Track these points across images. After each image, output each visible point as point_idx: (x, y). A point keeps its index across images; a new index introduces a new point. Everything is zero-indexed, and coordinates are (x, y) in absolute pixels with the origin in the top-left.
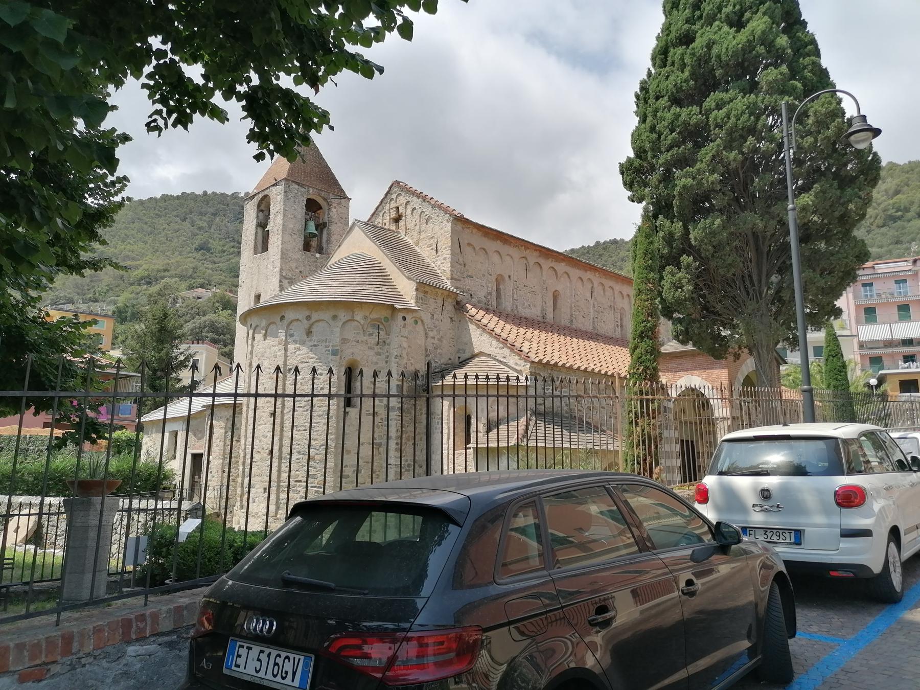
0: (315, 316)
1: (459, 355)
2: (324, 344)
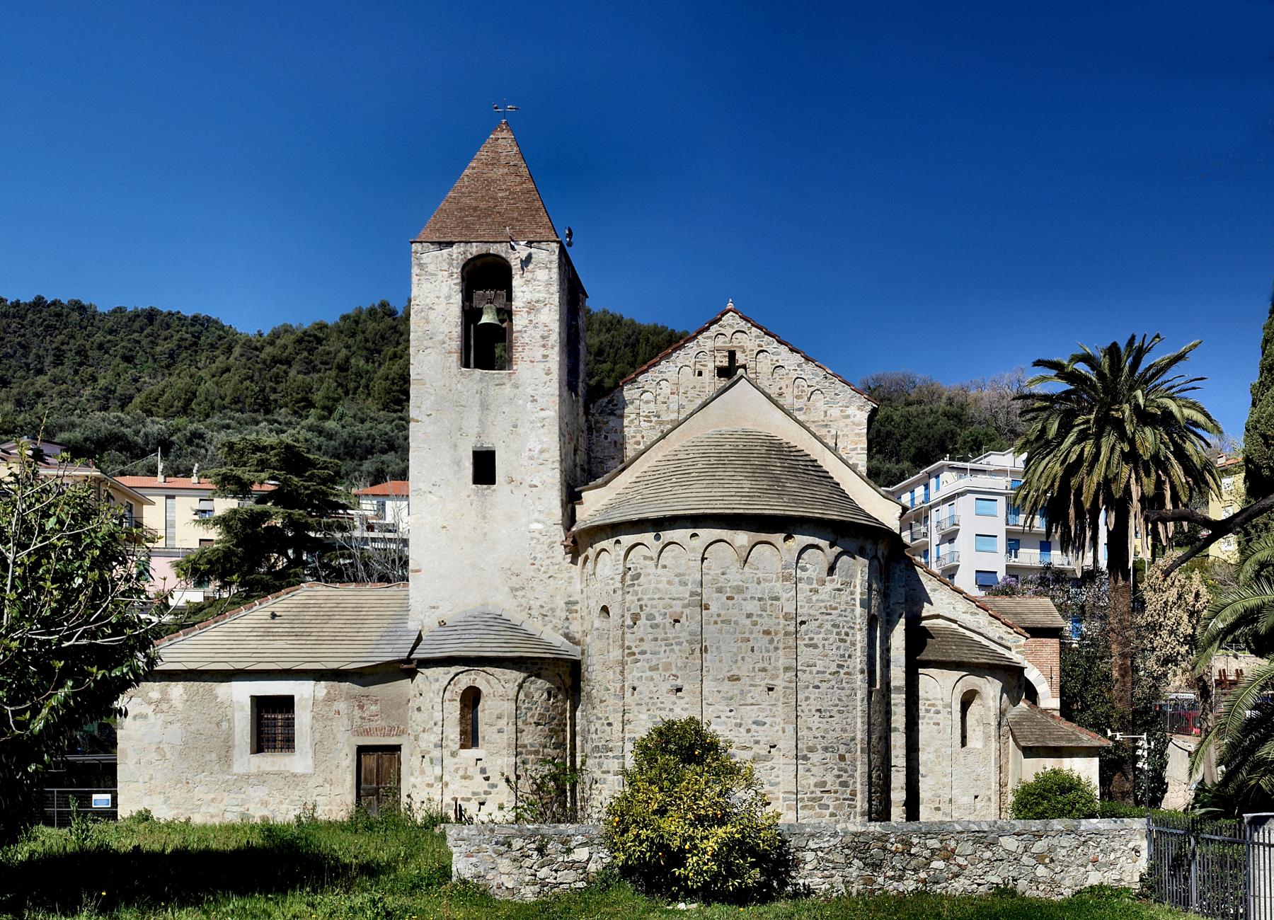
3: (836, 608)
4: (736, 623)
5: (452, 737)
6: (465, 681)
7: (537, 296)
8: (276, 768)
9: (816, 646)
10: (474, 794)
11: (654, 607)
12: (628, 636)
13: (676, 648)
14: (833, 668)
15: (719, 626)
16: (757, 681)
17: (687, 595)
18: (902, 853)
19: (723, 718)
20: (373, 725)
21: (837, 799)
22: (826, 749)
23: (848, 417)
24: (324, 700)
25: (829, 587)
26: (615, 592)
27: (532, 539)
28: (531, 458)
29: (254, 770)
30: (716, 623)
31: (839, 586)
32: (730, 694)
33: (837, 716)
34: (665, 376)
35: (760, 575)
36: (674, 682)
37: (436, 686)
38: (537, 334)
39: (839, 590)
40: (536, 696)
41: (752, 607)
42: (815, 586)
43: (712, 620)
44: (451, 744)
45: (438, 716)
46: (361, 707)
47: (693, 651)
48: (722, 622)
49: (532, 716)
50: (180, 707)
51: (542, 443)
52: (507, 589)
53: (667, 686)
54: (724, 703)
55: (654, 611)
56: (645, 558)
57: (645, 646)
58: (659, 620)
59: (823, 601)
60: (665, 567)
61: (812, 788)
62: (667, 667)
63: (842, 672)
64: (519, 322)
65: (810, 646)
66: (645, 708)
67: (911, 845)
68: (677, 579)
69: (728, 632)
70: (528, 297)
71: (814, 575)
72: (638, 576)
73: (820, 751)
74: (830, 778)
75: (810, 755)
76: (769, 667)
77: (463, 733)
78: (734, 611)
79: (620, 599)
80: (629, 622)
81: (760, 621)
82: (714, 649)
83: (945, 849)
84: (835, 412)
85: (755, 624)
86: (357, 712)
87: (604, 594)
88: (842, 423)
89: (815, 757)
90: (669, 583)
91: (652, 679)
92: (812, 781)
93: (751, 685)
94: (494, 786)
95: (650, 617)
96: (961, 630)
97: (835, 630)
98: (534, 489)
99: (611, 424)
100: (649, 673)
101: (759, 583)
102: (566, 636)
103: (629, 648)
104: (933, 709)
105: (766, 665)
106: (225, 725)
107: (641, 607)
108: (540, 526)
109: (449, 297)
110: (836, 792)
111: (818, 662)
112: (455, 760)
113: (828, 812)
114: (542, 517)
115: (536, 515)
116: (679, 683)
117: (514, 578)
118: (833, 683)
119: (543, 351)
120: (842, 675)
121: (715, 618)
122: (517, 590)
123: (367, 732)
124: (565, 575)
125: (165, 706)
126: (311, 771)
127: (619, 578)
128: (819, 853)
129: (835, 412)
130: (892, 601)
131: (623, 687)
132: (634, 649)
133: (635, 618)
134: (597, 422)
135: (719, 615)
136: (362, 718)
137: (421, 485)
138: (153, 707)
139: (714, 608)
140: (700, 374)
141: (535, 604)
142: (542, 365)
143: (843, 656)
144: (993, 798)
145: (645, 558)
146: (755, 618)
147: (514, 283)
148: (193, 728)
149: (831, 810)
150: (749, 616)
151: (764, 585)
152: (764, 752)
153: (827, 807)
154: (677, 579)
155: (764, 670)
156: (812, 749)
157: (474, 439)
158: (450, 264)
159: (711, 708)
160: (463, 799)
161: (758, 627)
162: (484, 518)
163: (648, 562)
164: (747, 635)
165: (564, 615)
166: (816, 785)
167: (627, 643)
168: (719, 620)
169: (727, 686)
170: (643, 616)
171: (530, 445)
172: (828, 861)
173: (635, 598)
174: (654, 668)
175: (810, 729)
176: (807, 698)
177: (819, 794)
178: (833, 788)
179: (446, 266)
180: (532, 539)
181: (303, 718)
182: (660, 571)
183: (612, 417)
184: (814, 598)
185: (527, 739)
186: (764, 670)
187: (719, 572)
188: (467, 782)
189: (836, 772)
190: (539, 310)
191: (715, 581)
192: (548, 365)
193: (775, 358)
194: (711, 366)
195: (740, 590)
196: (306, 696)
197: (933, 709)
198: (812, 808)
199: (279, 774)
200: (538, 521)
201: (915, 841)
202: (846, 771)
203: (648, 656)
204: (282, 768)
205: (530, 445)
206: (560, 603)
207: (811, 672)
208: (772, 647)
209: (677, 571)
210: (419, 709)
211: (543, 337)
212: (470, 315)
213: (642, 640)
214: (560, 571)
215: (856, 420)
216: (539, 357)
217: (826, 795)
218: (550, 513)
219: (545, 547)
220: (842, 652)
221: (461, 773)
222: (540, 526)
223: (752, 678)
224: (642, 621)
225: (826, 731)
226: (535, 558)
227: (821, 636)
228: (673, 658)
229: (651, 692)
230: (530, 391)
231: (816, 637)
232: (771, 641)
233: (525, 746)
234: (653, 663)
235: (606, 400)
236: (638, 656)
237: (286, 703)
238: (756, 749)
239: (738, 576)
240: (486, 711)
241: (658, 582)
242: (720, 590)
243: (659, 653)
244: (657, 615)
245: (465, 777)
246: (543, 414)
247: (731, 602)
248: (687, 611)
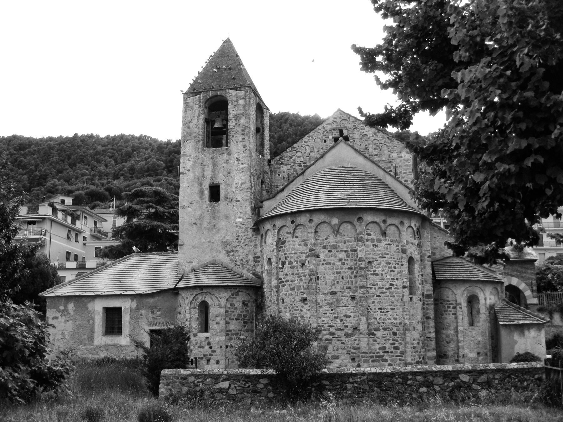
0: (389, 221)
2: (395, 244)
3: (387, 254)
4: (334, 264)
5: (194, 326)
6: (200, 298)
7: (239, 112)
8: (113, 343)
9: (377, 275)
10: (205, 355)
11: (292, 257)
12: (280, 273)
13: (303, 278)
14: (388, 286)
15: (325, 266)
16: (346, 294)
17: (308, 251)
18: (402, 384)
19: (328, 314)
20: (158, 321)
21: (393, 356)
22: (384, 329)
23: (401, 157)
24: (135, 309)
25: (383, 243)
26: (273, 251)
27: (237, 226)
28: (237, 187)
29: (103, 344)
30: (323, 264)
31: (389, 243)
32: (331, 301)
33: (391, 311)
34: (307, 144)
35: (346, 239)
36: (302, 296)
37: (187, 301)
38: (239, 129)
39: (389, 244)
40: (237, 305)
41: (342, 255)
42: (375, 243)
43: (321, 263)
44: (193, 330)
45: (188, 316)
46: (153, 312)
47: (311, 279)
48: (327, 264)
49: (234, 316)
50: (72, 313)
51: (242, 180)
52: (225, 252)
53: (298, 298)
54: (328, 306)
55: (292, 260)
56: (288, 233)
57: (288, 278)
58: (294, 264)
59: (380, 251)
60: (297, 237)
61: (378, 350)
62: (299, 288)
63: (393, 287)
64: (231, 124)
65: (374, 274)
66: (288, 310)
67: (408, 379)
68: (303, 243)
69: (330, 269)
70: (235, 113)
71: (375, 237)
72: (284, 242)
73: (382, 330)
74: (388, 345)
75: (375, 333)
76: (352, 287)
77: (200, 324)
78: (332, 258)
79: (276, 254)
80: (280, 266)
81: (346, 262)
82: (322, 278)
83: (427, 381)
84: (394, 155)
85: (343, 264)
86: (150, 315)
87: (269, 252)
88: (398, 160)
89: (379, 334)
90: (299, 245)
91: (292, 295)
92: (377, 346)
93: (342, 296)
94: (215, 351)
95: (290, 263)
97: (388, 266)
98: (238, 202)
99: (282, 169)
100: (290, 292)
101: (345, 243)
102: (253, 274)
103: (280, 279)
104: (452, 306)
105: (350, 285)
106: (91, 322)
107: (286, 258)
108: (241, 220)
109: (199, 116)
110: (392, 352)
111: (379, 283)
112: (196, 338)
113: (387, 364)
114: (242, 216)
115: (239, 215)
116: (305, 296)
117: (228, 246)
118: (388, 294)
119: (242, 137)
120: (393, 289)
121: (322, 262)
122: (230, 252)
123: (155, 325)
124: (253, 244)
125: (66, 313)
126: (129, 344)
127: (275, 244)
128: (355, 385)
129: (394, 155)
130: (424, 249)
131: (278, 300)
132: (283, 280)
133: (283, 263)
134: (275, 168)
135: (324, 260)
136: (153, 318)
137: (184, 204)
138: (61, 313)
139: (322, 257)
140: (325, 141)
141: (239, 259)
142: (242, 143)
143: (393, 279)
144: (488, 354)
145: (288, 233)
146: (343, 261)
147: (229, 107)
148: (77, 323)
149: (389, 362)
150: (340, 260)
151: (347, 244)
152: (350, 332)
153: (386, 361)
154: (303, 243)
155: (349, 288)
156: (377, 330)
157: (209, 180)
158: (200, 102)
159: (321, 309)
160: (199, 358)
161: (345, 266)
162: (214, 218)
163: (288, 235)
164: (339, 270)
165: (252, 263)
166: (380, 349)
167: (280, 277)
168: (324, 263)
169: (329, 297)
170: (287, 262)
171: (236, 180)
172: (360, 389)
173: (283, 253)
174: (293, 289)
175: (376, 319)
176: (373, 302)
177: (382, 354)
178: (389, 350)
179: (197, 103)
180: (237, 226)
181: (126, 318)
182: (295, 239)
183: (282, 165)
184: (375, 249)
185: (232, 327)
186: (349, 288)
187: (324, 238)
188: (201, 350)
189: (391, 341)
190: (240, 118)
191: (322, 243)
192: (244, 143)
193: (362, 131)
194: (330, 137)
195: (335, 247)
196: (127, 307)
197: (452, 306)
198: (378, 361)
199: (115, 345)
200: (240, 218)
201: (410, 377)
202: (397, 341)
203: (289, 283)
204: (116, 343)
205: (236, 180)
206: (251, 257)
207: (375, 289)
208: (353, 276)
209: (303, 238)
210: (180, 313)
211: (242, 130)
212: (209, 122)
213: (286, 275)
214: (251, 242)
215: (406, 158)
216: (240, 139)
217: (386, 354)
218: (246, 214)
219: (243, 230)
220: (392, 277)
221: (198, 345)
222: (241, 220)
223: (343, 293)
224: (287, 265)
225: (385, 319)
226: (239, 236)
227: (380, 269)
228: (302, 283)
229: (291, 301)
230: (236, 156)
231: (377, 270)
232: (352, 273)
233: (230, 331)
234: (292, 286)
235: (278, 157)
236: (285, 283)
237: (119, 310)
238: (346, 330)
239: (334, 240)
240: (213, 311)
241: (294, 245)
242: (324, 248)
243: (294, 281)
244: (293, 261)
245: (200, 347)
246: (242, 166)
247: (330, 254)
248: (309, 259)
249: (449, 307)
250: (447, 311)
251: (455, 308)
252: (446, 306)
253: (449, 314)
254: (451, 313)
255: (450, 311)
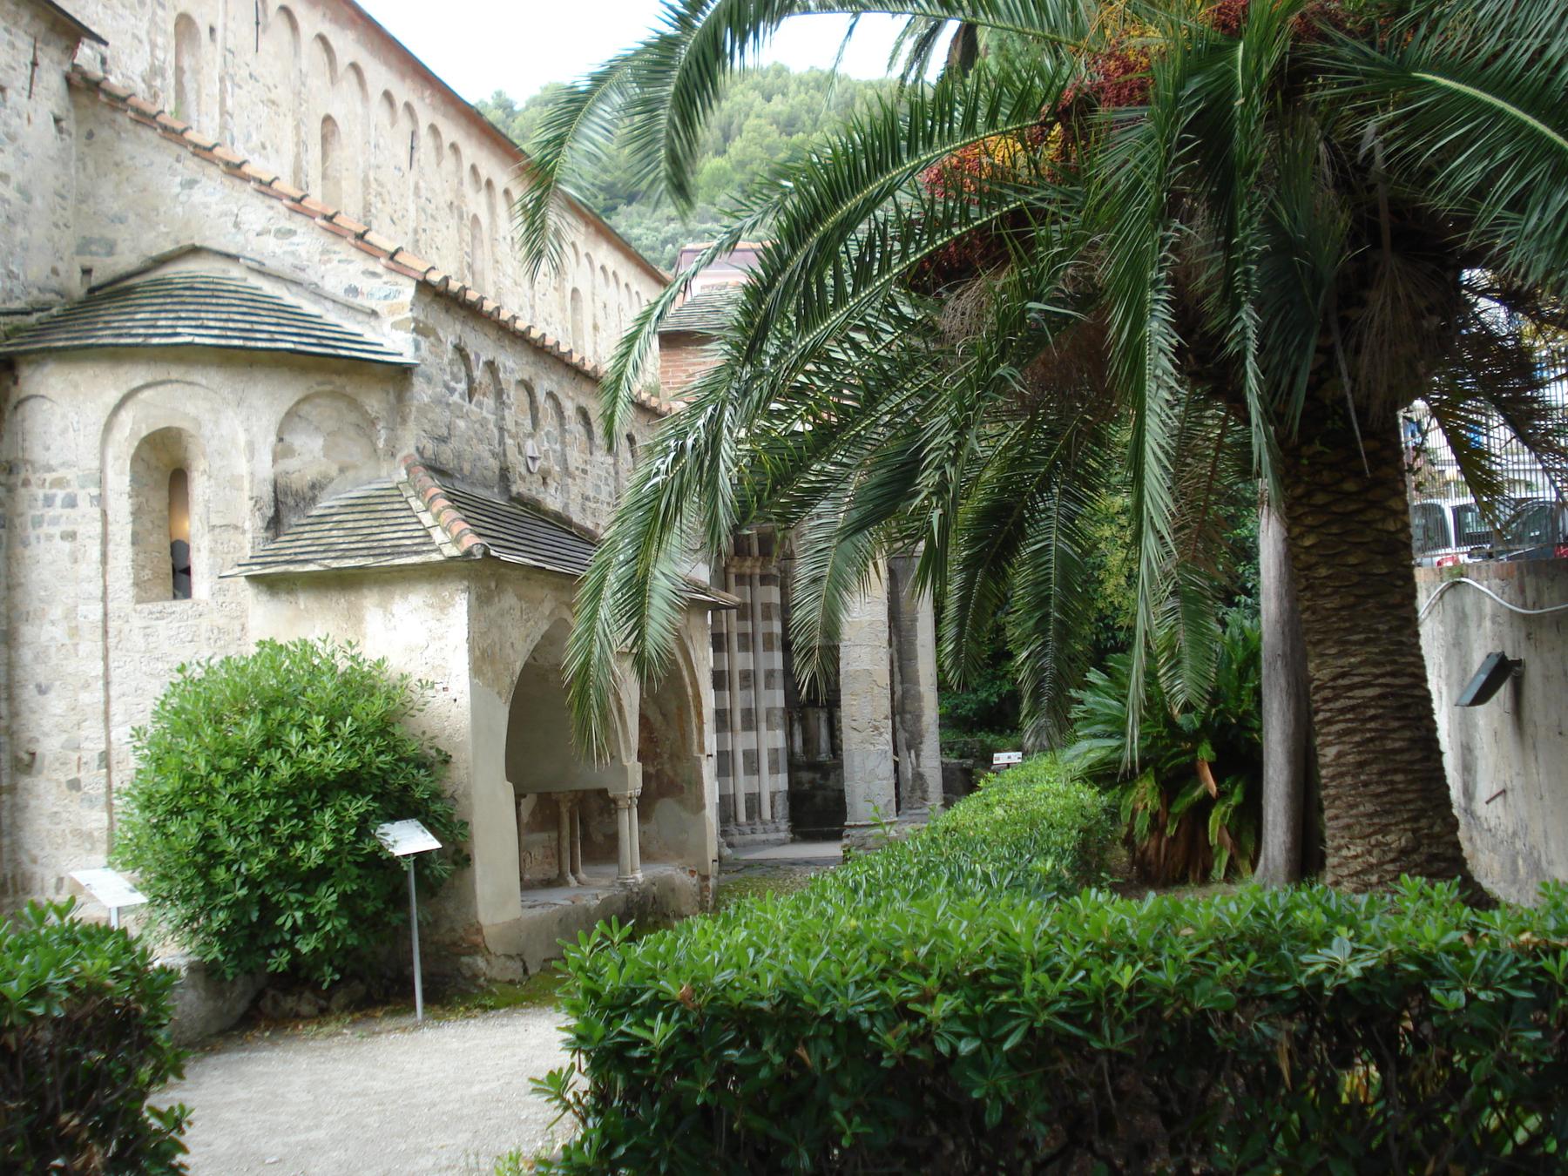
1: (87, 261)
96: (254, 281)
197: (60, 494)
249: (49, 501)
250: (38, 522)
251: (71, 503)
252: (40, 493)
253: (49, 537)
254: (56, 531)
255: (55, 521)
